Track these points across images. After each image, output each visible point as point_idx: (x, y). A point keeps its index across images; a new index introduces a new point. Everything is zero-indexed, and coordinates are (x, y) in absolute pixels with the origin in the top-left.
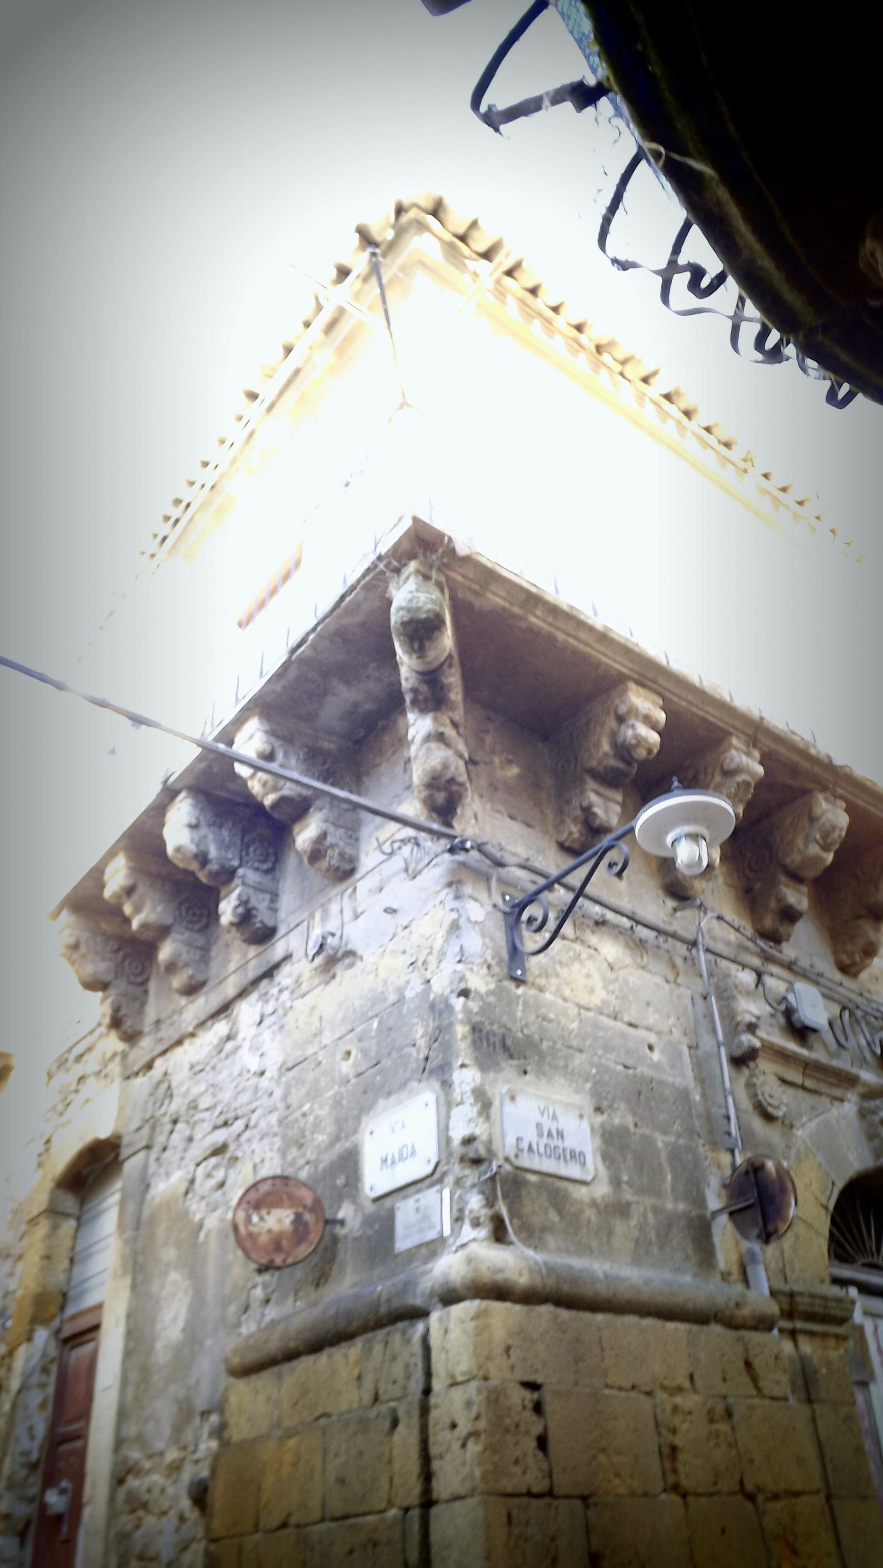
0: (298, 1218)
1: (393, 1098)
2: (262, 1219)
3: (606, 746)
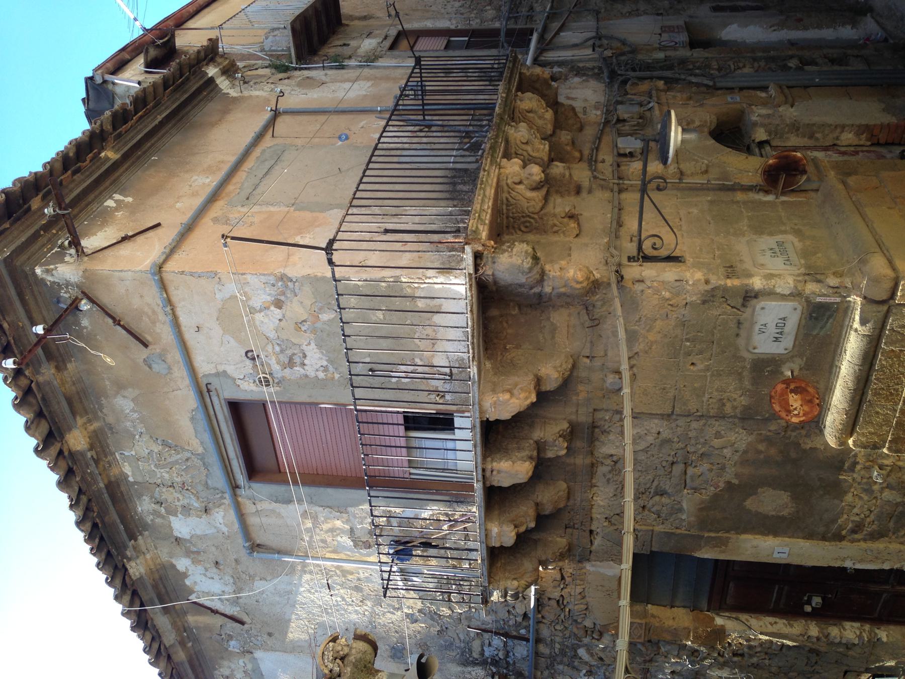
0: (792, 391)
1: (743, 333)
2: (795, 409)
3: (529, 194)
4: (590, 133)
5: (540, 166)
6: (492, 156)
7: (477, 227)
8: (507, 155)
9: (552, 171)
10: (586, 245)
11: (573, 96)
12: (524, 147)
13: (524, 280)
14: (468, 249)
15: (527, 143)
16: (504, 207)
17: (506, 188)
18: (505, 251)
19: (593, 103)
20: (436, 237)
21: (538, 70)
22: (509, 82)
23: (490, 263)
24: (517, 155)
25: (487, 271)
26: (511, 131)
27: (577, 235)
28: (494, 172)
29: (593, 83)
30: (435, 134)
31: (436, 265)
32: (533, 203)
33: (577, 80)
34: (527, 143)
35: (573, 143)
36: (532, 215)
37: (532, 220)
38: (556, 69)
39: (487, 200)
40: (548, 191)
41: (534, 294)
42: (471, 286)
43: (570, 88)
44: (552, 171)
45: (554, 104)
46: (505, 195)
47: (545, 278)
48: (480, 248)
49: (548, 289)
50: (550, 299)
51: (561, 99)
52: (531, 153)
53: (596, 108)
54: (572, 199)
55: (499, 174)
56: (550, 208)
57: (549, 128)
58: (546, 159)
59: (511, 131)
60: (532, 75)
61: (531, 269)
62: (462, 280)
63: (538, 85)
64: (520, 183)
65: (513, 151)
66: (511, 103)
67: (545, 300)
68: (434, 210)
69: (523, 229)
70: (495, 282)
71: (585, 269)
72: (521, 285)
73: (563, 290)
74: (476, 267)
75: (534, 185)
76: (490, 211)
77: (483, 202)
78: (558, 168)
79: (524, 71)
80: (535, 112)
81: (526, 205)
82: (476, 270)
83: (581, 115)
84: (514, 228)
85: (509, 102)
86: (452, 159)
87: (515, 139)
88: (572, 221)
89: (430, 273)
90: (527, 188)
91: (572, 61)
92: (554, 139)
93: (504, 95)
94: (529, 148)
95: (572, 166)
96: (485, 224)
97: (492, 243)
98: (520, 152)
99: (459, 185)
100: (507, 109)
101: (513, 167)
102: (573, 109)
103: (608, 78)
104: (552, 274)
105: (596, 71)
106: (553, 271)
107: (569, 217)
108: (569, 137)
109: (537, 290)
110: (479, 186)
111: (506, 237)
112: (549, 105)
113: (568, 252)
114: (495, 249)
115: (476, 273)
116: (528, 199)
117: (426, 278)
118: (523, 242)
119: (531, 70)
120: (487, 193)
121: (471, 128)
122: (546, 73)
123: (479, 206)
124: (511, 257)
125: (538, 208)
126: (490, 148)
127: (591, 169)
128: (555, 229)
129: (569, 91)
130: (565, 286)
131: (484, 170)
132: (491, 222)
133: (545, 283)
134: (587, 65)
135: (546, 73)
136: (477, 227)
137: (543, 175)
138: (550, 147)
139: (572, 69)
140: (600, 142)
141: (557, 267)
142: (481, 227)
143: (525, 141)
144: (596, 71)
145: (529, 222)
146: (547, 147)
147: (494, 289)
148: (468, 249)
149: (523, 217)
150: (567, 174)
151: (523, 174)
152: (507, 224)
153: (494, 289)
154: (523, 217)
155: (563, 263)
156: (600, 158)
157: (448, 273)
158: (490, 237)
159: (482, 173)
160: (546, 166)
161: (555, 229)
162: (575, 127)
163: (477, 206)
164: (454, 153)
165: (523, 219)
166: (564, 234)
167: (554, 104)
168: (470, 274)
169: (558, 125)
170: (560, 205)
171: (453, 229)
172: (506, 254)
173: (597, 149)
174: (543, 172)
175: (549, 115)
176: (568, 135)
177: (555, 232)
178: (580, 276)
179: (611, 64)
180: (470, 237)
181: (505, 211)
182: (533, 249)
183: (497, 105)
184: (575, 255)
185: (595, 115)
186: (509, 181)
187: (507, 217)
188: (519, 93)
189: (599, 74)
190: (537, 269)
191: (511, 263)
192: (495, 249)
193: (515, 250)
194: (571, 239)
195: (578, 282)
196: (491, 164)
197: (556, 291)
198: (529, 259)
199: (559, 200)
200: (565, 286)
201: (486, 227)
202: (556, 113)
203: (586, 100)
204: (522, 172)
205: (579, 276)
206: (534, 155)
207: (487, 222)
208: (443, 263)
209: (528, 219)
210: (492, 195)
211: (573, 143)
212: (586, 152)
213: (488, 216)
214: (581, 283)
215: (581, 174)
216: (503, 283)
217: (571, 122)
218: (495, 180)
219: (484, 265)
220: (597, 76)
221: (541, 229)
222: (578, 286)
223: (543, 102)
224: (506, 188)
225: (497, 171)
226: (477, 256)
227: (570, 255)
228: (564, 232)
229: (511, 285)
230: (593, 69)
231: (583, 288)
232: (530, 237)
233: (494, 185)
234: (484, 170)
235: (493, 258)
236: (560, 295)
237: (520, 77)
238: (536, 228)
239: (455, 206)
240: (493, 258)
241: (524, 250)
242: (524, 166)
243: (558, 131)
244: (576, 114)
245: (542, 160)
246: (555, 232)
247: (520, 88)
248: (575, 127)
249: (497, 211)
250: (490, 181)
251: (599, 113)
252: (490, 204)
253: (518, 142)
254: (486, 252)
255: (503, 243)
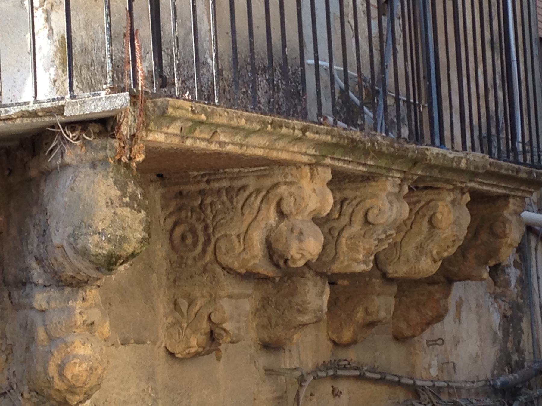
3: (257, 237)
4: (390, 357)
5: (320, 255)
6: (336, 146)
7: (174, 119)
8: (339, 180)
9: (310, 284)
10: (151, 377)
11: (464, 315)
12: (359, 218)
13: (57, 240)
14: (122, 100)
15: (367, 222)
16: (225, 184)
17: (268, 182)
18: (123, 188)
19: (452, 359)
20: (145, 31)
21: (515, 235)
22: (489, 174)
23: (92, 155)
24: (341, 203)
25: (73, 151)
26: (389, 185)
27: (172, 355)
28: (301, 153)
29: (491, 353)
30: (374, 23)
31: (78, 35)
32: (238, 248)
33: (496, 319)
34: (367, 222)
35: (371, 325)
36: (210, 249)
37: (199, 248)
38: (513, 274)
39: (238, 139)
40: (266, 279)
41: (27, 270)
42: (34, 114)
43: (478, 306)
44: (310, 284)
45: (448, 275)
46: (252, 183)
47: (68, 290)
48: (125, 130)
49: (39, 299)
50: (17, 307)
51: (458, 289)
52: (346, 234)
53: (442, 366)
54: (251, 336)
55: (297, 165)
56: (229, 286)
57: (398, 269)
58: (336, 268)
59: (389, 185)
60: (505, 222)
61: (84, 253)
62: (47, 93)
63: (484, 236)
64: (281, 214)
65: (349, 193)
66: (448, 181)
67: (15, 294)
68: (205, 26)
69: (179, 231)
70: (47, 174)
71: (93, 381)
72: (44, 233)
73: (41, 334)
74: (81, 124)
75: (279, 247)
76: (214, 147)
77: (233, 132)
78: (316, 296)
79: (512, 204)
80: (431, 236)
81: (234, 233)
82: (72, 125)
83: (427, 335)
84: (180, 209)
85: (449, 176)
86: (324, 63)
87: (374, 196)
88: (203, 339)
89: (59, 19)
90: (271, 230)
91: (531, 305)
92: (377, 282)
93: (463, 165)
94: (356, 227)
95: (323, 325)
96: (183, 138)
97: (140, 158)
98: (347, 209)
99: (268, 79)
100: (436, 173)
101: (314, 194)
102: (439, 318)
103: (504, 384)
104: (78, 305)
105: (515, 357)
106: (85, 307)
107: (212, 333)
108: (382, 314)
109: (37, 274)
110: (269, 118)
111: (157, 193)
112: (447, 262)
113: (131, 337)
114: (127, 166)
115: (64, 125)
116: (247, 237)
117: (47, 12)
118: (148, 229)
119: (514, 219)
120: (254, 140)
121: (390, 102)
122: (508, 255)
123: (223, 120)
124: (111, 203)
125: (226, 260)
126: (353, 140)
127: (317, 369)
128: (184, 304)
129: (473, 306)
130: (51, 338)
131: (304, 130)
132: (188, 155)
133: (54, 293)
134: (524, 337)
135: (508, 255)
136: (174, 119)
137: (301, 263)
138: (361, 274)
139: (516, 307)
140: (375, 381)
141: (95, 315)
142: (174, 129)
143: (371, 218)
144: (515, 357)
145: (195, 244)
146: (362, 268)
147: (33, 173)
148: (122, 100)
149: (206, 228)
150: (306, 318)
151: (302, 221)
152: (185, 190)
153: (33, 173)
154: (206, 228)
155: (106, 329)
156: (343, 386)
157: (63, 63)
158: (154, 154)
159: (298, 124)
160: (318, 268)
161: (184, 304)
162: (403, 326)
163: (223, 116)
164: (338, 67)
165: (200, 227)
166: (173, 325)
167: (448, 275)
168: (60, 110)
169: (406, 287)
170: (237, 309)
171: (166, 71)
172: (115, 192)
173: (361, 378)
174: (307, 264)
175: (428, 266)
176: (387, 310)
177: (176, 303)
178: (76, 370)
179: (530, 387)
180: (150, 104)
181: (216, 185)
182: (133, 255)
183: (441, 151)
184: (126, 354)
185: (428, 367)
186: (283, 189)
187: (202, 192)
188: (467, 198)
189: (509, 364)
190: (84, 268)
191: (93, 203)
192: (127, 166)
193: (127, 211)
194: (163, 341)
195: (61, 369)
196: (318, 145)
197: (38, 319)
198: (107, 248)
199: (247, 305)
200: (51, 338)
201: (176, 141)
202: (430, 281)
203: (457, 342)
204: (306, 215)
205: (77, 370)
206: (343, 240)
207: (189, 143)
208: (85, 51)
209: (202, 240)
210: (250, 152)
211: (371, 325)
212: (352, 355)
213: (202, 145)
214: (61, 375)
215: (307, 349)
216: (46, 189)
217: (413, 315)
218: (284, 156)
219: (85, 143)
220: (506, 362)
221: (180, 270)
222: (52, 370)
223: (452, 250)
224: (268, 182)
225: (305, 159)
226: (106, 124)
227: (125, 343)
228: (177, 323)
229: (45, 211)
230: (519, 351)
231: (50, 381)
232: (161, 249)
233: (274, 155)
234: (304, 130)
235: (104, 161)
236: (28, 329)
237: (499, 197)
238: (181, 262)
239: (220, 72)
240: (104, 161)
241: (128, 233)
242: (319, 221)
243: (394, 289)
244: (429, 324)
245: (334, 260)
246: (176, 303)
247: (478, 199)
248: (403, 326)
249: (216, 165)
250: (281, 144)
251: (434, 372)
252: (230, 148)
253: (368, 203)
254: (116, 143)
255: (139, 183)
